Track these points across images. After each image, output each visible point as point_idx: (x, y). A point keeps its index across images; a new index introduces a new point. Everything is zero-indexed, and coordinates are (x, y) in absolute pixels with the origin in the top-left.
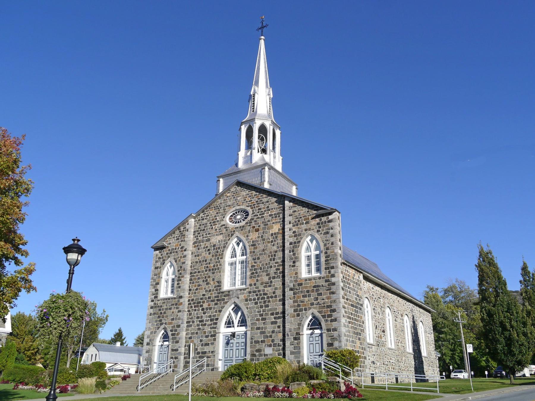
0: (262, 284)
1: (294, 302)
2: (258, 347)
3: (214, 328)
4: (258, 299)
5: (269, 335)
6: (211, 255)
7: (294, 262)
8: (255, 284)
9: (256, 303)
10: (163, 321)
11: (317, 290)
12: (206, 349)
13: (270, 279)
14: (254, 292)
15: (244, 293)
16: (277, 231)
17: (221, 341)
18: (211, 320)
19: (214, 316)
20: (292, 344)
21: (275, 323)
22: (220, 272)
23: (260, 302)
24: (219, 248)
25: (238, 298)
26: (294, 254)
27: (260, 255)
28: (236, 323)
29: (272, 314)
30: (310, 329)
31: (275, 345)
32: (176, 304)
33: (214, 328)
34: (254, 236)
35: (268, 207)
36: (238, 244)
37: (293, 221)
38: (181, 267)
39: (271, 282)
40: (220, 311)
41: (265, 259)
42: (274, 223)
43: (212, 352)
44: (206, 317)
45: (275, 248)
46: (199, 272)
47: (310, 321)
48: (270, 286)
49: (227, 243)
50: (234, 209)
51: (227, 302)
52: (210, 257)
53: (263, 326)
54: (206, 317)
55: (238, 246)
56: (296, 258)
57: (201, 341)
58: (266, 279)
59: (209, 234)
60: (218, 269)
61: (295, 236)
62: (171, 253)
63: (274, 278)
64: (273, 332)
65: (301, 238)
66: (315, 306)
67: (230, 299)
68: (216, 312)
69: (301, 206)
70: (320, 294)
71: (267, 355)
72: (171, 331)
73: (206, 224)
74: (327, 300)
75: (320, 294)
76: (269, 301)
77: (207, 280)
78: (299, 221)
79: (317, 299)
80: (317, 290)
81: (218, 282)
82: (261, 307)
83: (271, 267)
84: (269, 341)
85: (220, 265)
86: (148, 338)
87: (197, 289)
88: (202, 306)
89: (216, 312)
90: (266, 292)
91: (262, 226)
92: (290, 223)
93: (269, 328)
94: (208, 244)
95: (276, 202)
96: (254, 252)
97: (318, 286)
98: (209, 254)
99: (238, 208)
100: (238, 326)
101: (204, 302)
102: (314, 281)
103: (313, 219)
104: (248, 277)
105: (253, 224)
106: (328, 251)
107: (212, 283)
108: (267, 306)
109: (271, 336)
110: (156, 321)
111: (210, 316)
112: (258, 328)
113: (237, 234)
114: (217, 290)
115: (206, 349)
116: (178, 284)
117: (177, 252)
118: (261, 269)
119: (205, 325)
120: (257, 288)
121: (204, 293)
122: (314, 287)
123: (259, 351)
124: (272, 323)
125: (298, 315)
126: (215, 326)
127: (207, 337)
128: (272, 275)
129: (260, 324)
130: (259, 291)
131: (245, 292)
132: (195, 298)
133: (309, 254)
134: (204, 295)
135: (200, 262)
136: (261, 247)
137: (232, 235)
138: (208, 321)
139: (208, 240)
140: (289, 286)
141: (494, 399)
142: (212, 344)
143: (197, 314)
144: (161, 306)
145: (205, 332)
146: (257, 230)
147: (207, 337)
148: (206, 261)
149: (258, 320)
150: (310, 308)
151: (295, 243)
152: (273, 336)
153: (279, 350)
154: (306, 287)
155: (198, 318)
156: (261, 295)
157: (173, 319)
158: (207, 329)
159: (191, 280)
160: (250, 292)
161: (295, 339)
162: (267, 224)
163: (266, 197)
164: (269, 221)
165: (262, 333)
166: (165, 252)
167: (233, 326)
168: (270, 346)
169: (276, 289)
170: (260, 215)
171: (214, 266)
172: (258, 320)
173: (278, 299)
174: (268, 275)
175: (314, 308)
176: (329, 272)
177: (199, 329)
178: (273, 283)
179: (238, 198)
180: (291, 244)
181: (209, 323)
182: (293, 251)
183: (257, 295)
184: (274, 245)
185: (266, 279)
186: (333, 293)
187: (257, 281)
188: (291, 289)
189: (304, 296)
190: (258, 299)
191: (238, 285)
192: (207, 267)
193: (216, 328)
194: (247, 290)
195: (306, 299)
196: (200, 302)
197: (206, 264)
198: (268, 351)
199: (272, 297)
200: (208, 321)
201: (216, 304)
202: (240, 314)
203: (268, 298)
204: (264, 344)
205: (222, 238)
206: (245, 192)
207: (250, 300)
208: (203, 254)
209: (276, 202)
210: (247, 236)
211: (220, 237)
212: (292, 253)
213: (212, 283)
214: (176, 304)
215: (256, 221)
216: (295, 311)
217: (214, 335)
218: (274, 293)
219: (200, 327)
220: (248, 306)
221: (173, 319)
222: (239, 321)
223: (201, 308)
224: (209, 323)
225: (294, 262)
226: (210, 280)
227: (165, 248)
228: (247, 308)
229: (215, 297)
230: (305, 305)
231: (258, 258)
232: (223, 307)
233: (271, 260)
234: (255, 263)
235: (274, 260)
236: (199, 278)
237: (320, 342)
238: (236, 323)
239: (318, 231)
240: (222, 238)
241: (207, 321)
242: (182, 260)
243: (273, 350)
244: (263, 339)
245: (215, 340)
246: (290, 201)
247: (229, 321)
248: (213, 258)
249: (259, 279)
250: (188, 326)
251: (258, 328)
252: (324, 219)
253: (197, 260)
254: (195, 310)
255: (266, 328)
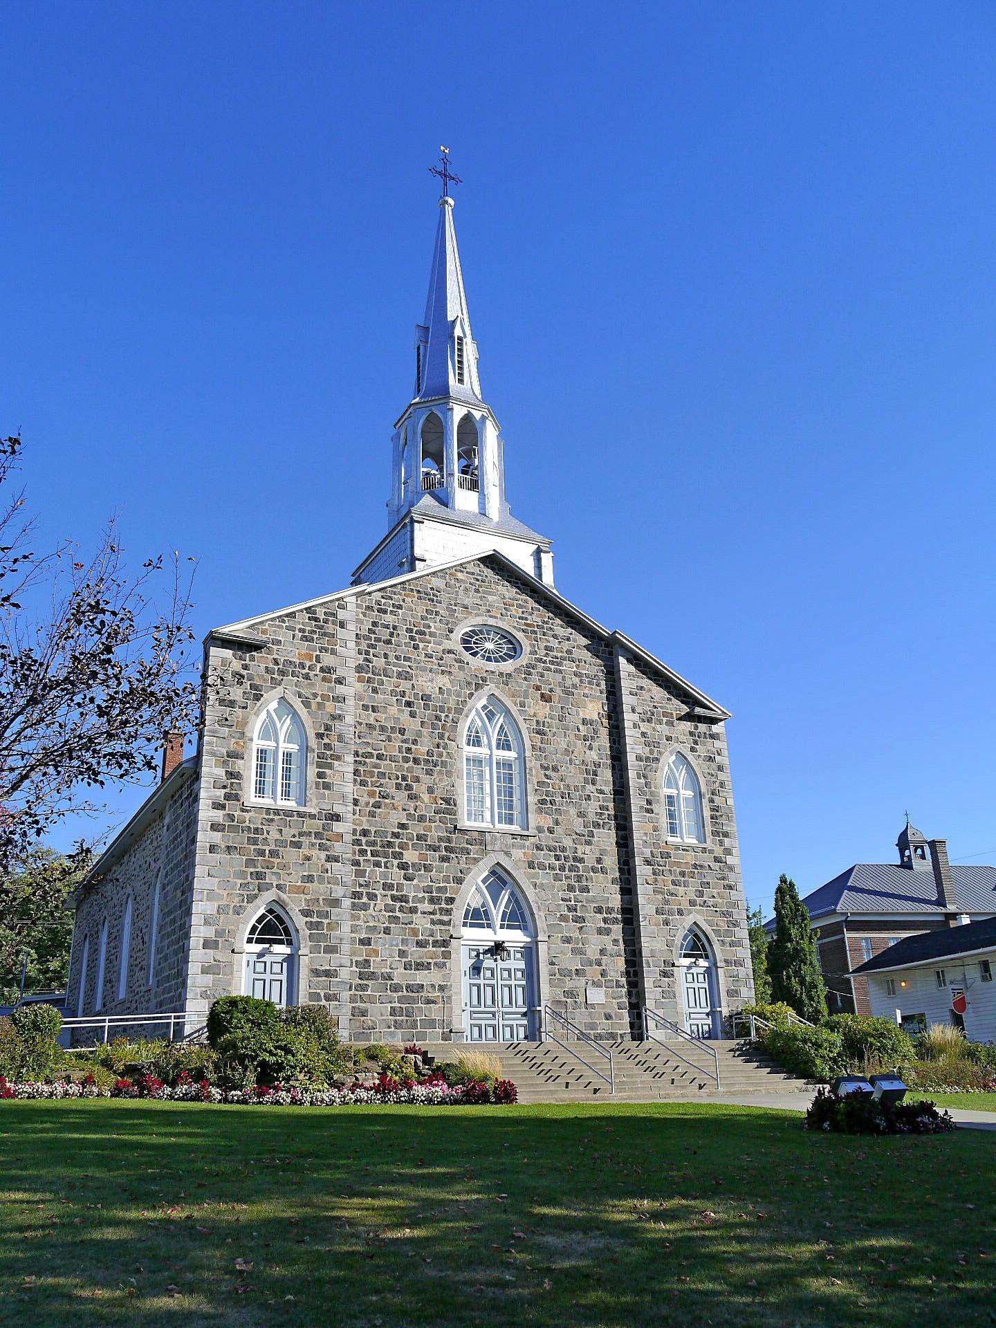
2: (569, 984)
3: (441, 922)
4: (562, 868)
6: (418, 720)
10: (270, 879)
12: (421, 977)
17: (462, 960)
18: (432, 901)
21: (608, 932)
22: (449, 774)
24: (442, 709)
25: (508, 854)
28: (496, 915)
30: (259, 941)
33: (441, 922)
36: (491, 716)
39: (591, 834)
40: (459, 881)
41: (575, 777)
42: (585, 695)
43: (442, 988)
44: (417, 888)
46: (379, 757)
47: (259, 921)
48: (588, 843)
50: (480, 620)
51: (476, 860)
54: (417, 888)
57: (402, 954)
60: (444, 764)
65: (660, 753)
67: (485, 852)
69: (655, 681)
72: (306, 913)
73: (395, 628)
77: (409, 787)
79: (701, 894)
81: (447, 801)
84: (593, 972)
86: (207, 923)
88: (398, 856)
90: (579, 854)
94: (405, 685)
95: (587, 647)
99: (491, 622)
103: (679, 719)
104: (532, 808)
106: (716, 798)
107: (426, 797)
110: (242, 875)
111: (428, 890)
112: (568, 940)
113: (491, 688)
115: (421, 977)
116: (320, 775)
119: (413, 910)
121: (405, 821)
123: (570, 994)
124: (600, 931)
126: (446, 918)
127: (420, 944)
128: (592, 817)
129: (571, 929)
130: (563, 849)
131: (527, 843)
132: (373, 830)
133: (269, 744)
134: (403, 826)
135: (383, 729)
140: (643, 853)
141: (556, 1120)
142: (441, 966)
143: (385, 875)
145: (415, 932)
147: (420, 944)
151: (647, 759)
152: (603, 962)
153: (621, 997)
154: (678, 864)
155: (387, 887)
157: (310, 879)
158: (421, 923)
161: (665, 974)
166: (259, 664)
167: (489, 926)
169: (603, 852)
170: (552, 663)
172: (563, 918)
173: (610, 877)
178: (596, 839)
179: (490, 598)
180: (639, 758)
181: (426, 906)
183: (557, 858)
188: (648, 863)
190: (562, 868)
195: (681, 890)
196: (390, 844)
198: (597, 996)
200: (422, 900)
201: (444, 859)
202: (505, 896)
204: (583, 980)
206: (507, 591)
208: (393, 710)
209: (587, 647)
212: (643, 781)
213: (426, 797)
217: (445, 943)
218: (599, 861)
221: (310, 879)
222: (504, 913)
223: (396, 862)
224: (426, 906)
225: (649, 802)
226: (420, 789)
227: (258, 648)
228: (535, 885)
237: (284, 977)
238: (496, 915)
239: (693, 750)
243: (607, 994)
245: (447, 955)
246: (629, 661)
248: (425, 731)
251: (568, 940)
252: (702, 727)
253: (372, 721)
254: (377, 864)
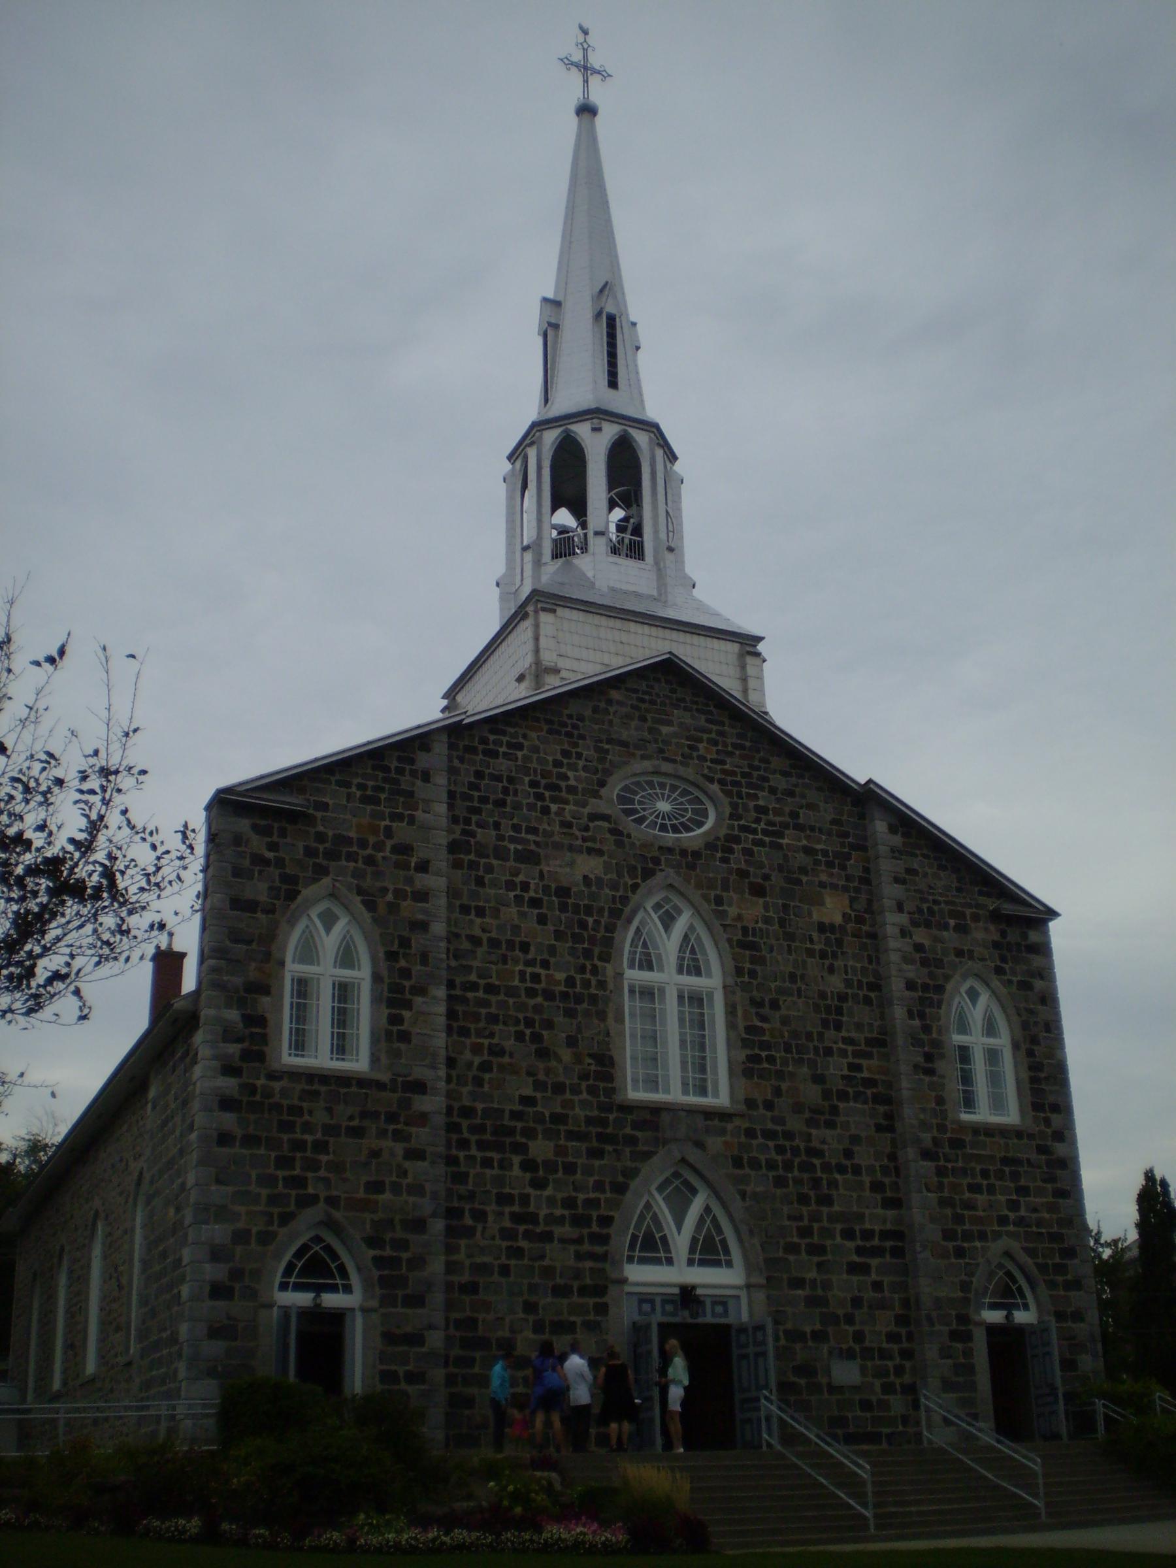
1: (943, 1202)
3: (593, 1256)
4: (788, 1166)
5: (840, 1312)
9: (780, 1182)
11: (1015, 1176)
13: (827, 1095)
14: (769, 1135)
15: (723, 1132)
16: (838, 919)
18: (577, 1221)
19: (592, 1203)
21: (864, 1269)
23: (798, 1182)
24: (589, 910)
25: (700, 1145)
26: (926, 1029)
31: (867, 1353)
32: (392, 1117)
33: (593, 1256)
34: (753, 910)
38: (405, 943)
44: (551, 1201)
45: (836, 983)
46: (491, 989)
48: (830, 1125)
49: (625, 900)
51: (648, 1155)
53: (812, 1274)
55: (667, 927)
56: (391, 1003)
60: (594, 999)
62: (332, 855)
63: (843, 1096)
64: (857, 1302)
65: (947, 978)
66: (1011, 1228)
68: (599, 1186)
70: (1023, 1191)
71: (840, 1389)
74: (1047, 1216)
75: (1023, 1191)
76: (833, 1184)
78: (931, 911)
79: (1014, 1205)
80: (1015, 1176)
82: (803, 1199)
83: (829, 1052)
85: (602, 985)
87: (485, 1067)
89: (599, 1186)
90: (815, 1144)
96: (752, 974)
97: (1016, 1162)
100: (690, 1262)
101: (530, 1133)
102: (1002, 1141)
108: (827, 1200)
109: (850, 1319)
114: (592, 1091)
117: (370, 861)
118: (788, 1049)
119: (547, 1237)
120: (780, 1121)
122: (1005, 1161)
123: (806, 1370)
124: (853, 1268)
125: (960, 1253)
126: (599, 1249)
130: (789, 1135)
131: (730, 1126)
134: (527, 1101)
137: (648, 874)
138: (561, 1221)
144: (296, 1110)
148: (525, 947)
149: (793, 1248)
150: (997, 1235)
151: (926, 988)
156: (796, 1151)
159: (451, 1015)
160: (750, 1133)
161: (954, 1335)
162: (799, 882)
168: (850, 1355)
169: (855, 1139)
171: (570, 981)
172: (793, 1248)
174: (818, 1079)
175: (1010, 1234)
177: (518, 1253)
179: (665, 730)
183: (780, 1150)
184: (831, 970)
185: (811, 1093)
187: (778, 1092)
188: (926, 1155)
189: (975, 1188)
193: (604, 1257)
194: (737, 1122)
195: (981, 1199)
197: (529, 963)
203: (826, 1167)
205: (599, 871)
207: (755, 1164)
210: (719, 901)
211: (590, 866)
214: (392, 1117)
216: (948, 1235)
218: (848, 1154)
219: (524, 1244)
220: (749, 1189)
224: (566, 1230)
225: (929, 1057)
228: (743, 1195)
229: (589, 1121)
231: (775, 1005)
232: (630, 1174)
234: (764, 1019)
236: (493, 1019)
239: (999, 971)
240: (599, 871)
241: (551, 1220)
242: (408, 908)
243: (863, 1369)
244: (818, 1327)
247: (709, 1239)
248: (563, 947)
249: (784, 1086)
250: (450, 1231)
254: (487, 1163)
255: (827, 1285)
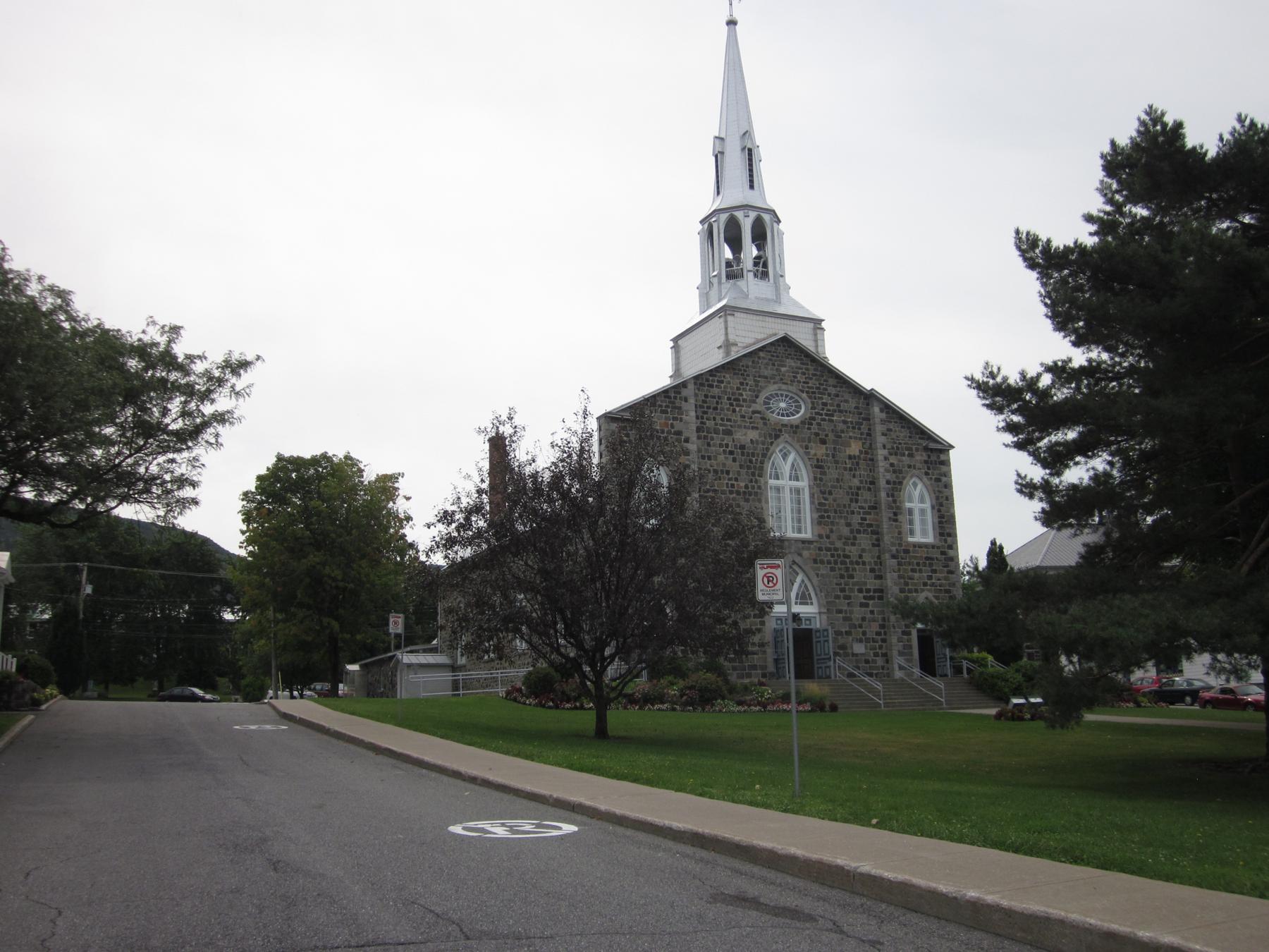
0: (840, 538)
1: (900, 577)
2: (841, 641)
4: (836, 563)
7: (895, 514)
8: (828, 537)
9: (832, 569)
11: (931, 565)
13: (852, 531)
14: (828, 549)
16: (857, 453)
20: (900, 640)
21: (867, 605)
24: (753, 455)
25: (800, 555)
26: (895, 501)
27: (833, 487)
29: (860, 591)
31: (867, 640)
35: (838, 405)
37: (889, 446)
41: (841, 496)
45: (856, 482)
48: (853, 544)
49: (768, 449)
52: (735, 467)
58: (845, 531)
59: (729, 420)
60: (756, 494)
61: (894, 472)
63: (859, 532)
64: (863, 619)
70: (934, 571)
75: (934, 571)
76: (854, 569)
79: (930, 578)
80: (931, 565)
82: (842, 577)
85: (759, 487)
91: (831, 436)
92: (884, 447)
93: (858, 613)
94: (728, 440)
97: (932, 559)
98: (734, 460)
105: (815, 428)
106: (943, 509)
108: (852, 577)
112: (840, 612)
122: (927, 558)
123: (843, 647)
124: (862, 605)
130: (836, 549)
136: (832, 474)
137: (777, 437)
139: (728, 433)
146: (823, 442)
148: (728, 472)
149: (837, 597)
150: (923, 591)
154: (916, 557)
156: (839, 556)
160: (820, 549)
163: (835, 386)
164: (842, 431)
165: (845, 619)
168: (861, 641)
169: (863, 550)
171: (746, 487)
172: (837, 597)
174: (848, 525)
176: (946, 541)
180: (888, 482)
182: (893, 496)
185: (845, 531)
186: (951, 572)
187: (832, 531)
188: (894, 557)
190: (836, 563)
191: (807, 534)
192: (733, 486)
195: (916, 575)
197: (730, 479)
199: (858, 563)
203: (852, 563)
207: (822, 562)
210: (807, 448)
211: (753, 435)
215: (819, 424)
218: (860, 556)
225: (895, 514)
230: (915, 584)
231: (830, 493)
233: (851, 500)
235: (857, 501)
239: (927, 474)
247: (803, 593)
248: (743, 471)
252: (934, 458)
255: (851, 612)
